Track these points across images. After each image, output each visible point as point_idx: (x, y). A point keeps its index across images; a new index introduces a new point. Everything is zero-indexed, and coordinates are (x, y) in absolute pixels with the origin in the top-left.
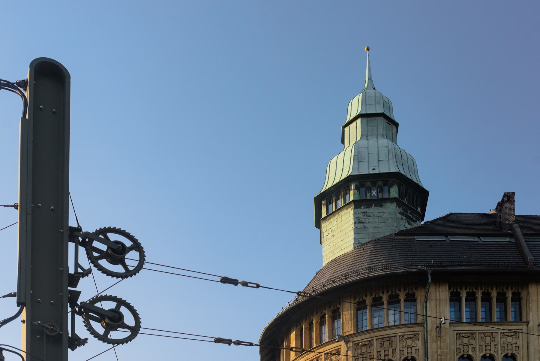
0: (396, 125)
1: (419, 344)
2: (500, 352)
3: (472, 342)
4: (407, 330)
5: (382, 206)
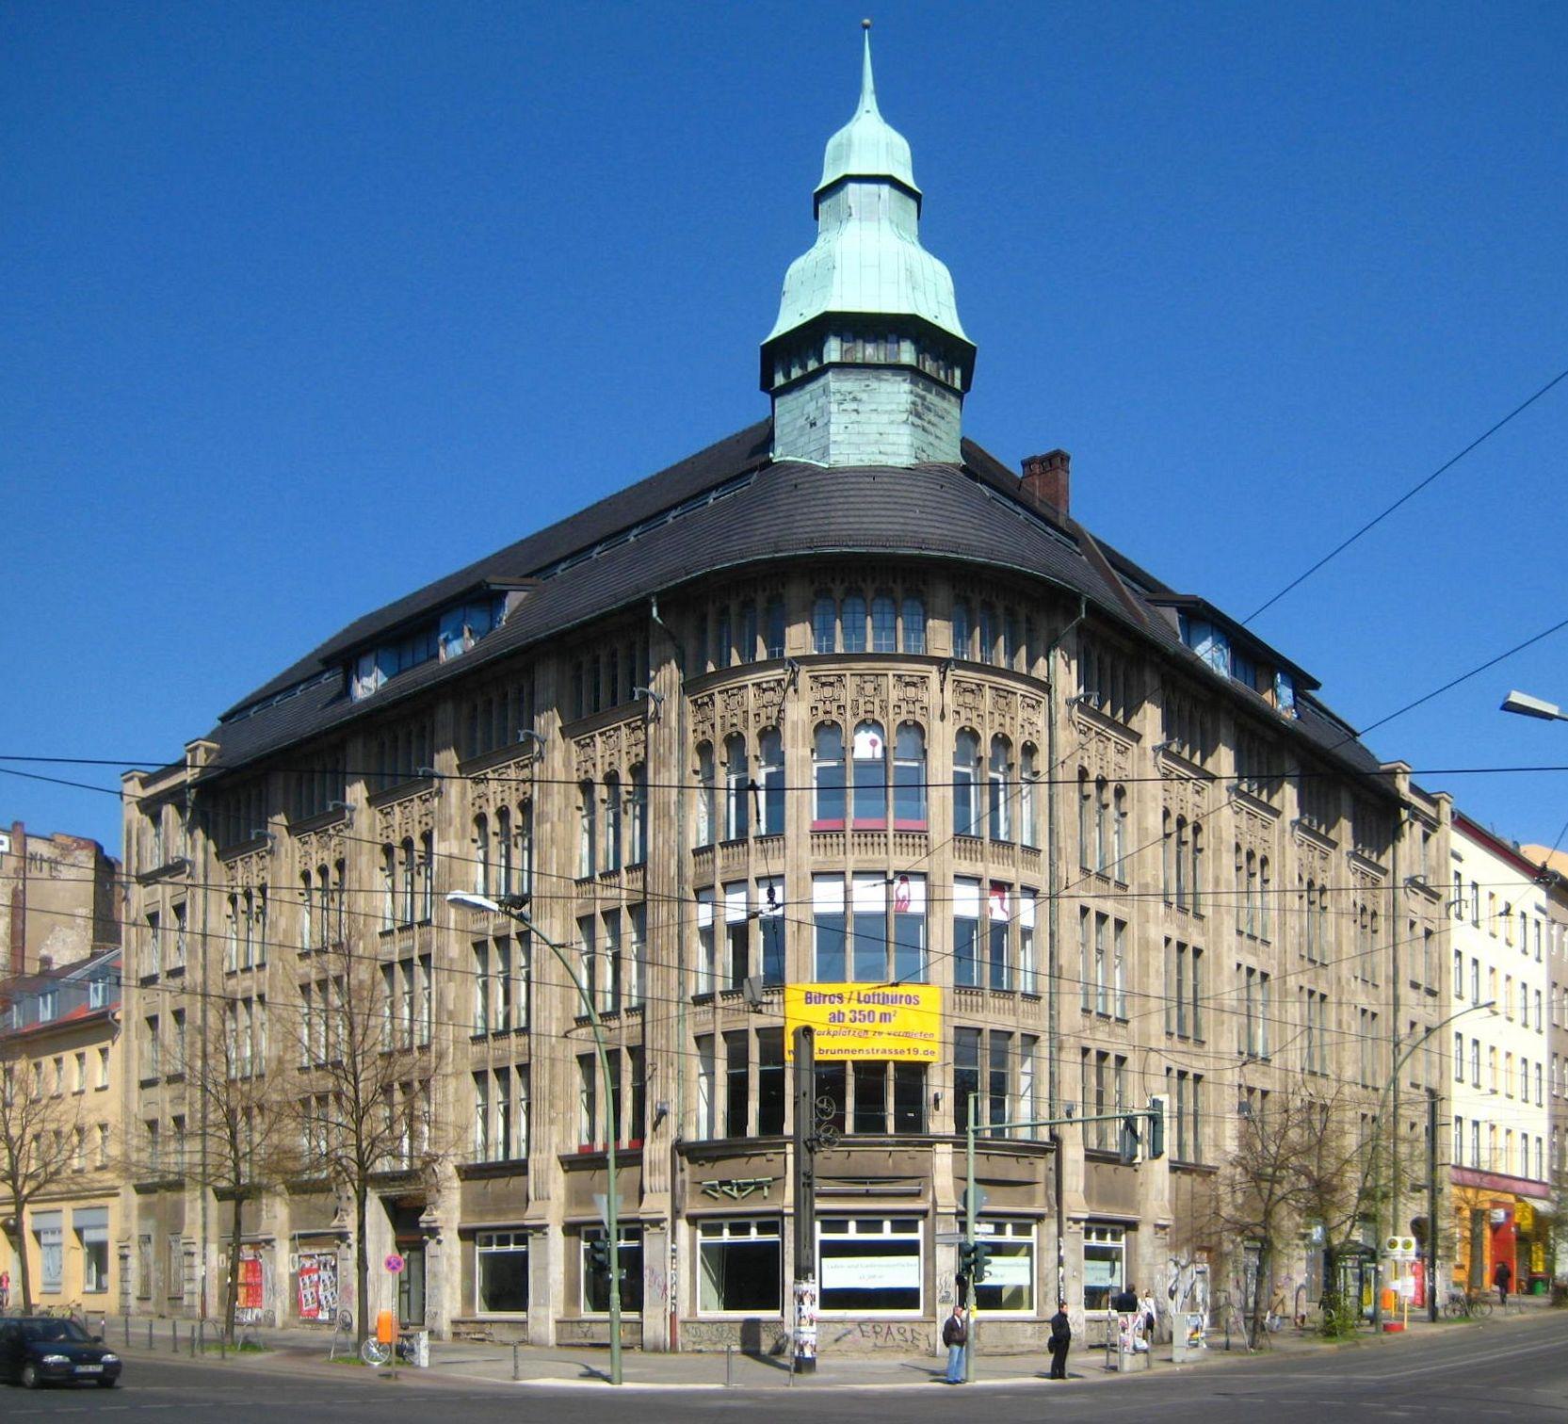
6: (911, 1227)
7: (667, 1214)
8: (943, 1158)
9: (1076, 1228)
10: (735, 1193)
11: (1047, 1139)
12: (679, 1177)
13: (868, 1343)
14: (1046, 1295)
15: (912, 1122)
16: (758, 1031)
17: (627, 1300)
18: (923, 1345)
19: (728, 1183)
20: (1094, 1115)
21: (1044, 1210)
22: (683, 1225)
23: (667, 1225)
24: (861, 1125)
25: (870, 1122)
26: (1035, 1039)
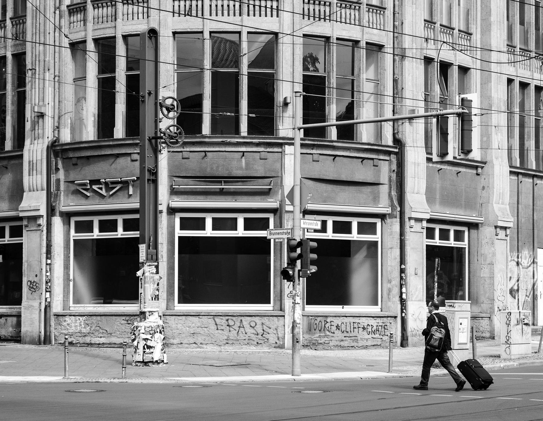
6: (263, 224)
7: (43, 211)
8: (292, 157)
9: (417, 227)
10: (103, 192)
11: (390, 143)
12: (53, 178)
13: (222, 336)
14: (390, 290)
15: (264, 123)
16: (125, 37)
17: (462, 252)
18: (272, 339)
19: (97, 182)
20: (389, 114)
21: (388, 210)
22: (57, 221)
23: (43, 222)
24: (253, 128)
25: (226, 125)
26: (380, 47)
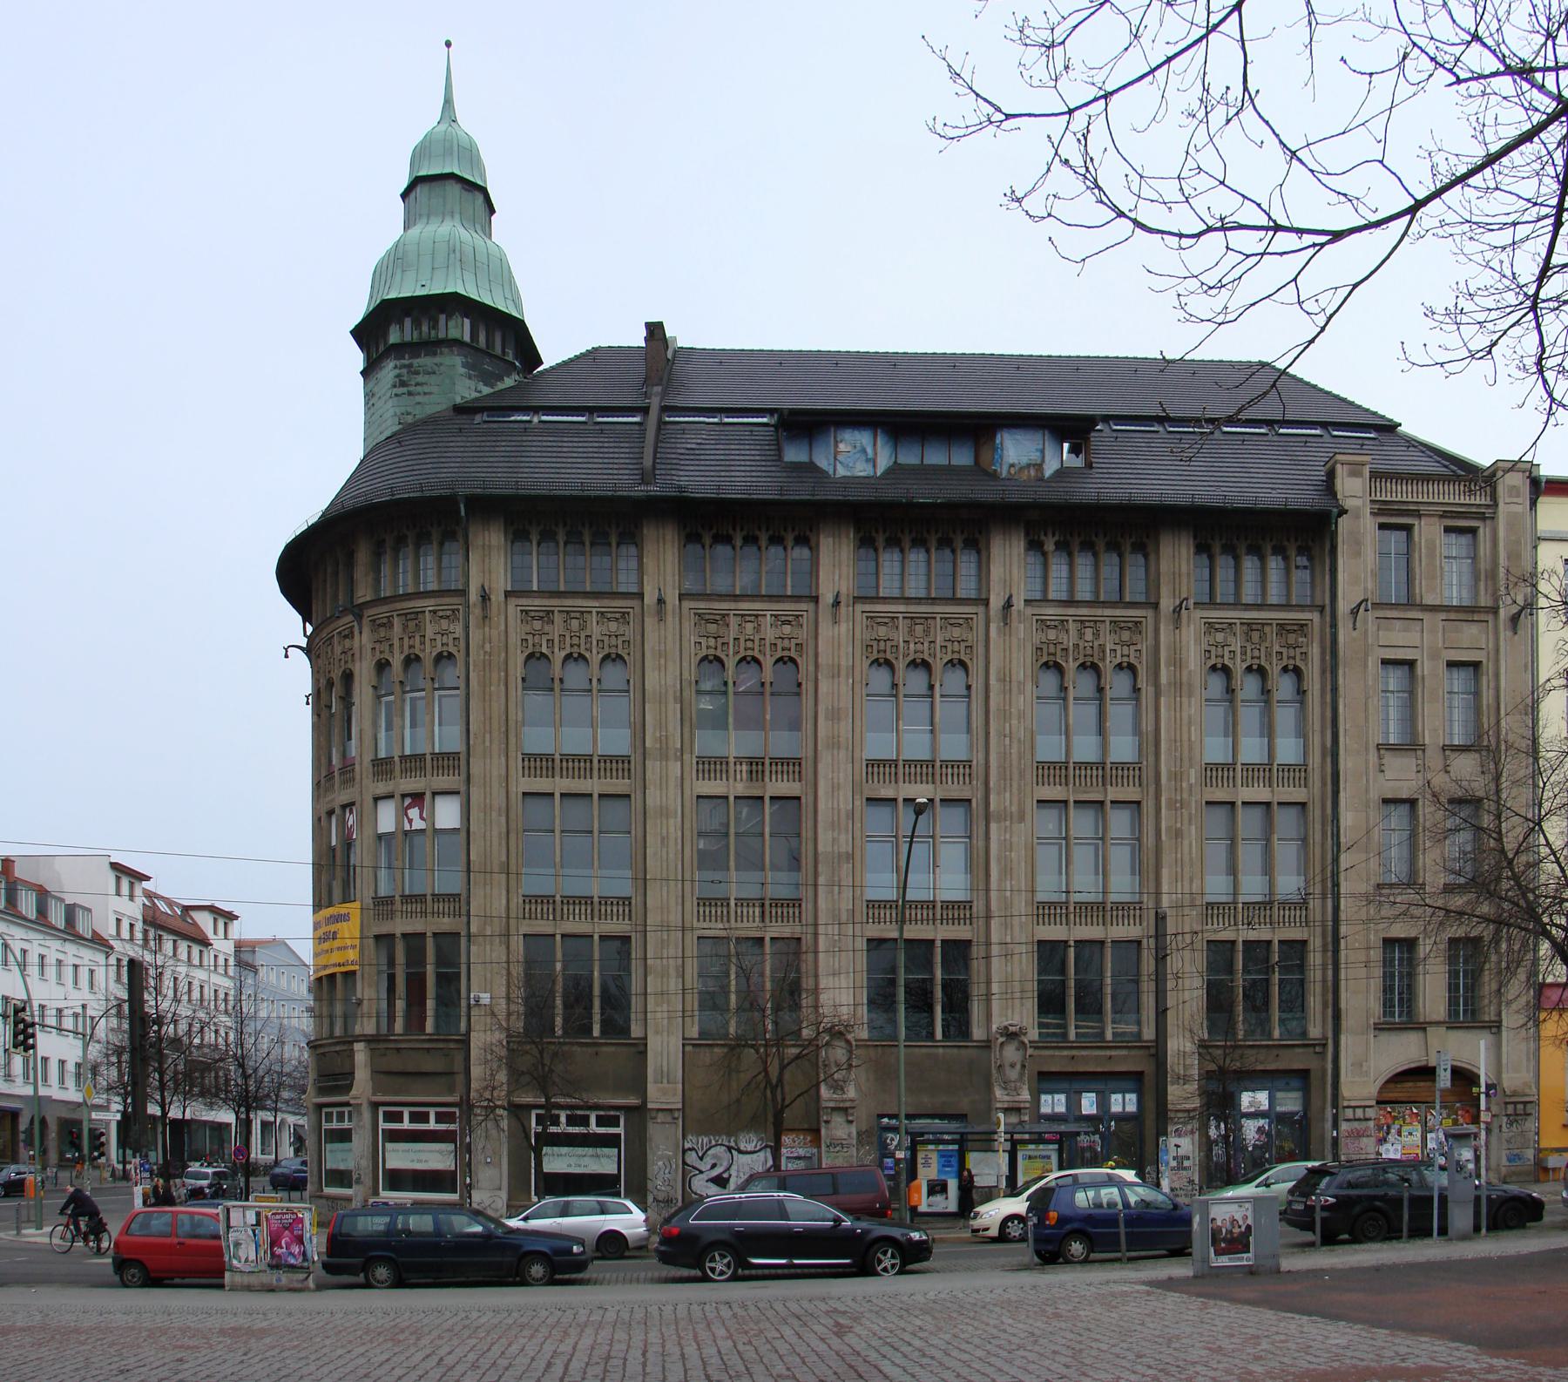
0: (492, 211)
1: (458, 629)
2: (768, 652)
3: (547, 628)
4: (439, 601)
5: (435, 354)
6: (614, 1122)
